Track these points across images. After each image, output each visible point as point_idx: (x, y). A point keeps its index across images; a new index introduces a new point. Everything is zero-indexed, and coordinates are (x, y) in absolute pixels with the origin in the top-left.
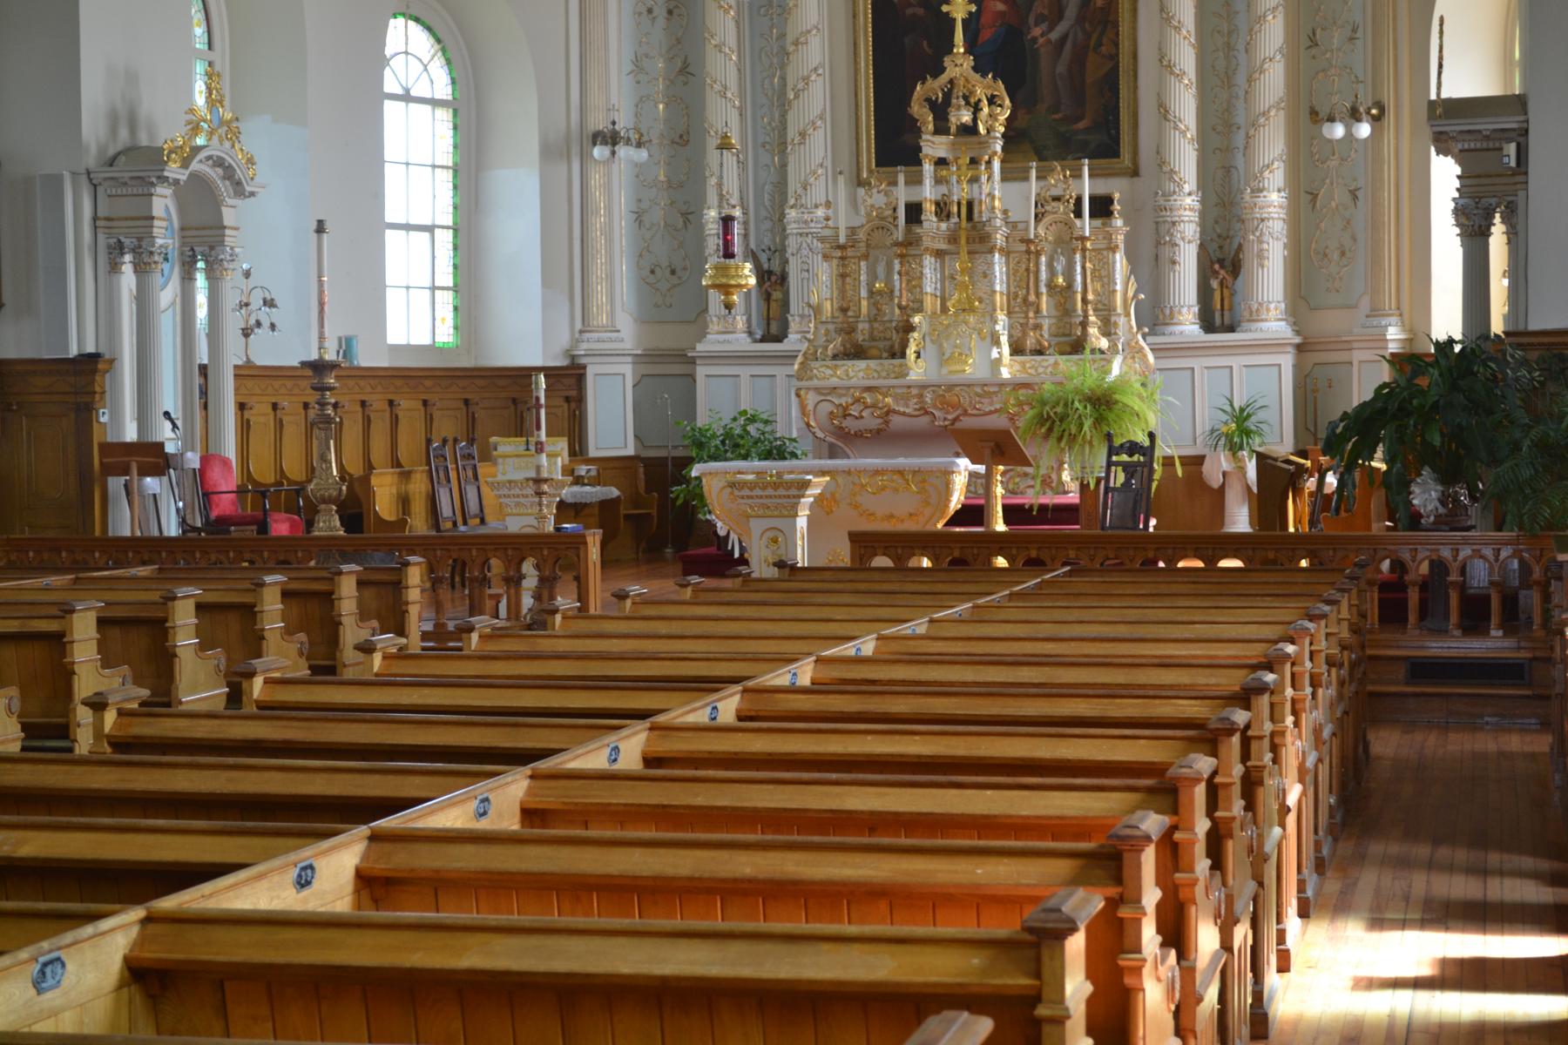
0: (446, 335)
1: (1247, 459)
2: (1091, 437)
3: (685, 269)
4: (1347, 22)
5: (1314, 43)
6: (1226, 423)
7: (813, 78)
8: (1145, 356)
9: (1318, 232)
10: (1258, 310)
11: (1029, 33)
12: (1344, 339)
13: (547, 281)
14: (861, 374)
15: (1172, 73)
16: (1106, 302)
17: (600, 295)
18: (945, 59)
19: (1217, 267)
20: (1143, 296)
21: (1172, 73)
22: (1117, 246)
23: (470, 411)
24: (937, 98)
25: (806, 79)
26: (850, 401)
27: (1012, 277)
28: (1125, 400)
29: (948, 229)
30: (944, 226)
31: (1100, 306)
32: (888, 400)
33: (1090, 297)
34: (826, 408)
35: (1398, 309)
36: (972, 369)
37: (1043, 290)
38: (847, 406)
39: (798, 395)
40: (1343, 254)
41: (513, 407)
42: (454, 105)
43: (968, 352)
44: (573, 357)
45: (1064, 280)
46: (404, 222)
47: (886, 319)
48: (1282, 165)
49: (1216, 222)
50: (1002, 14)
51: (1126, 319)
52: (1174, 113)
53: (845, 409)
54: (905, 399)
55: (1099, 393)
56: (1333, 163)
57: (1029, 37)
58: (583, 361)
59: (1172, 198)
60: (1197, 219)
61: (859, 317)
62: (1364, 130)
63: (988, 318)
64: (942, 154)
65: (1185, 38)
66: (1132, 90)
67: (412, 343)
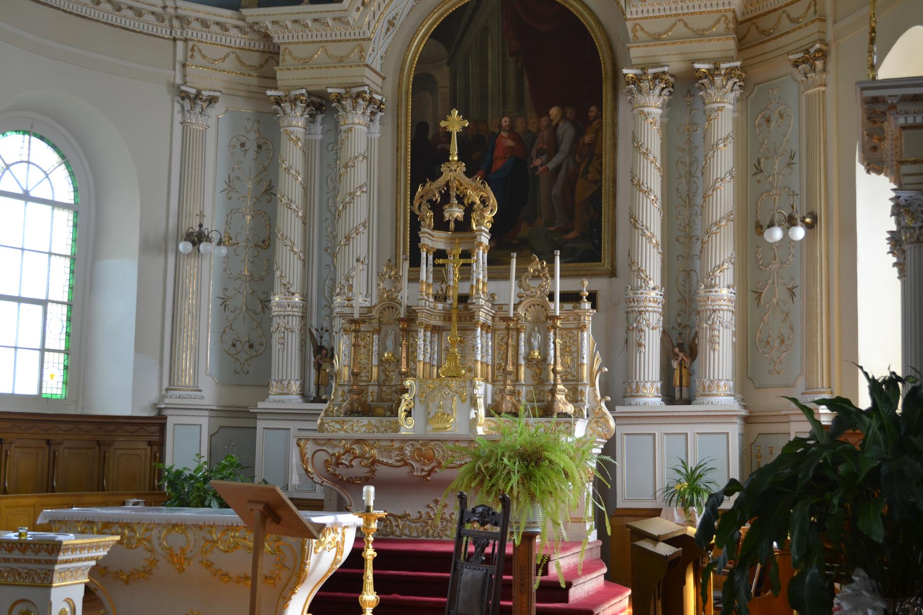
0: (55, 387)
1: (696, 515)
2: (518, 493)
3: (261, 344)
4: (786, 151)
5: (758, 170)
6: (679, 481)
7: (358, 194)
8: (607, 421)
9: (762, 324)
10: (709, 386)
11: (532, 163)
12: (783, 413)
13: (140, 346)
14: (364, 429)
15: (641, 190)
16: (575, 373)
17: (186, 362)
18: (443, 165)
19: (677, 350)
20: (606, 370)
21: (641, 190)
22: (585, 326)
23: (52, 450)
24: (436, 200)
25: (352, 195)
26: (342, 451)
27: (497, 351)
28: (553, 457)
29: (444, 309)
30: (440, 306)
31: (570, 377)
32: (373, 452)
33: (559, 368)
34: (322, 457)
35: (830, 387)
36: (454, 426)
37: (522, 362)
38: (339, 456)
39: (299, 445)
40: (783, 341)
41: (97, 448)
42: (75, 208)
43: (450, 413)
44: (160, 410)
45: (540, 354)
46: (17, 295)
47: (392, 384)
48: (731, 266)
49: (679, 315)
50: (509, 147)
51: (592, 389)
52: (642, 222)
53: (338, 458)
54: (388, 451)
55: (529, 450)
56: (775, 266)
57: (531, 166)
58: (166, 413)
59: (639, 292)
60: (660, 310)
61: (370, 382)
62: (799, 233)
63: (468, 384)
64: (441, 246)
65: (652, 162)
66: (611, 207)
67: (17, 392)
